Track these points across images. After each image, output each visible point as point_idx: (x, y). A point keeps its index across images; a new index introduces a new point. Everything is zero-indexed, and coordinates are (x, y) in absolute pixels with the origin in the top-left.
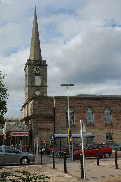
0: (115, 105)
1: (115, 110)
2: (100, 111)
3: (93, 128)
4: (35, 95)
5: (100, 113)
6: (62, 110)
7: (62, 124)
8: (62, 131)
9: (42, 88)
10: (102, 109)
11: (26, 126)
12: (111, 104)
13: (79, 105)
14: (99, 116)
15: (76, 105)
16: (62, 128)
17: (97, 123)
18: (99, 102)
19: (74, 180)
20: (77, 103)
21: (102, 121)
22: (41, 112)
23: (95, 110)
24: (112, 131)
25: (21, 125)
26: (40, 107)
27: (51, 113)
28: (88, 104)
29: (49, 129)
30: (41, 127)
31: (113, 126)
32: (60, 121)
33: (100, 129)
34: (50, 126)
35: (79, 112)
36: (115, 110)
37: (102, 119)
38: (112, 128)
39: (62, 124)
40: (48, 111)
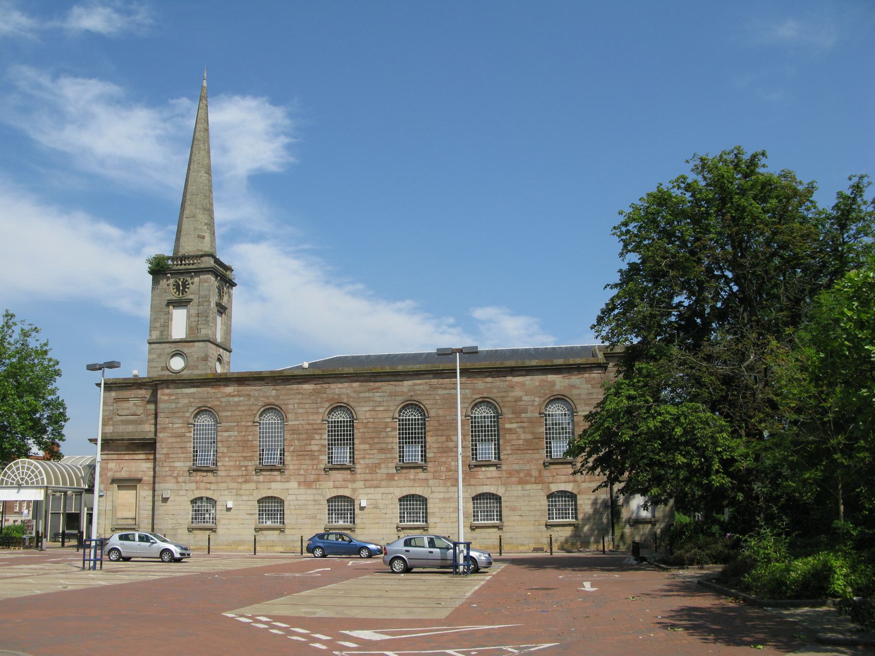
0: (371, 395)
1: (368, 415)
2: (311, 418)
3: (279, 478)
4: (167, 368)
5: (310, 427)
6: (177, 421)
7: (176, 464)
8: (175, 486)
9: (193, 346)
10: (318, 413)
11: (9, 469)
12: (354, 392)
13: (236, 399)
14: (305, 436)
15: (224, 400)
16: (176, 478)
17: (297, 462)
18: (307, 387)
19: (786, 612)
20: (229, 395)
21: (316, 454)
22: (121, 427)
23: (290, 416)
24: (354, 490)
25: (28, 469)
26: (119, 412)
27: (147, 429)
28: (267, 397)
29: (139, 480)
30: (120, 475)
31: (358, 471)
32: (171, 456)
33: (308, 484)
34: (145, 469)
35: (234, 424)
36: (368, 415)
37: (315, 448)
38: (354, 481)
39: (176, 464)
40: (141, 423)
